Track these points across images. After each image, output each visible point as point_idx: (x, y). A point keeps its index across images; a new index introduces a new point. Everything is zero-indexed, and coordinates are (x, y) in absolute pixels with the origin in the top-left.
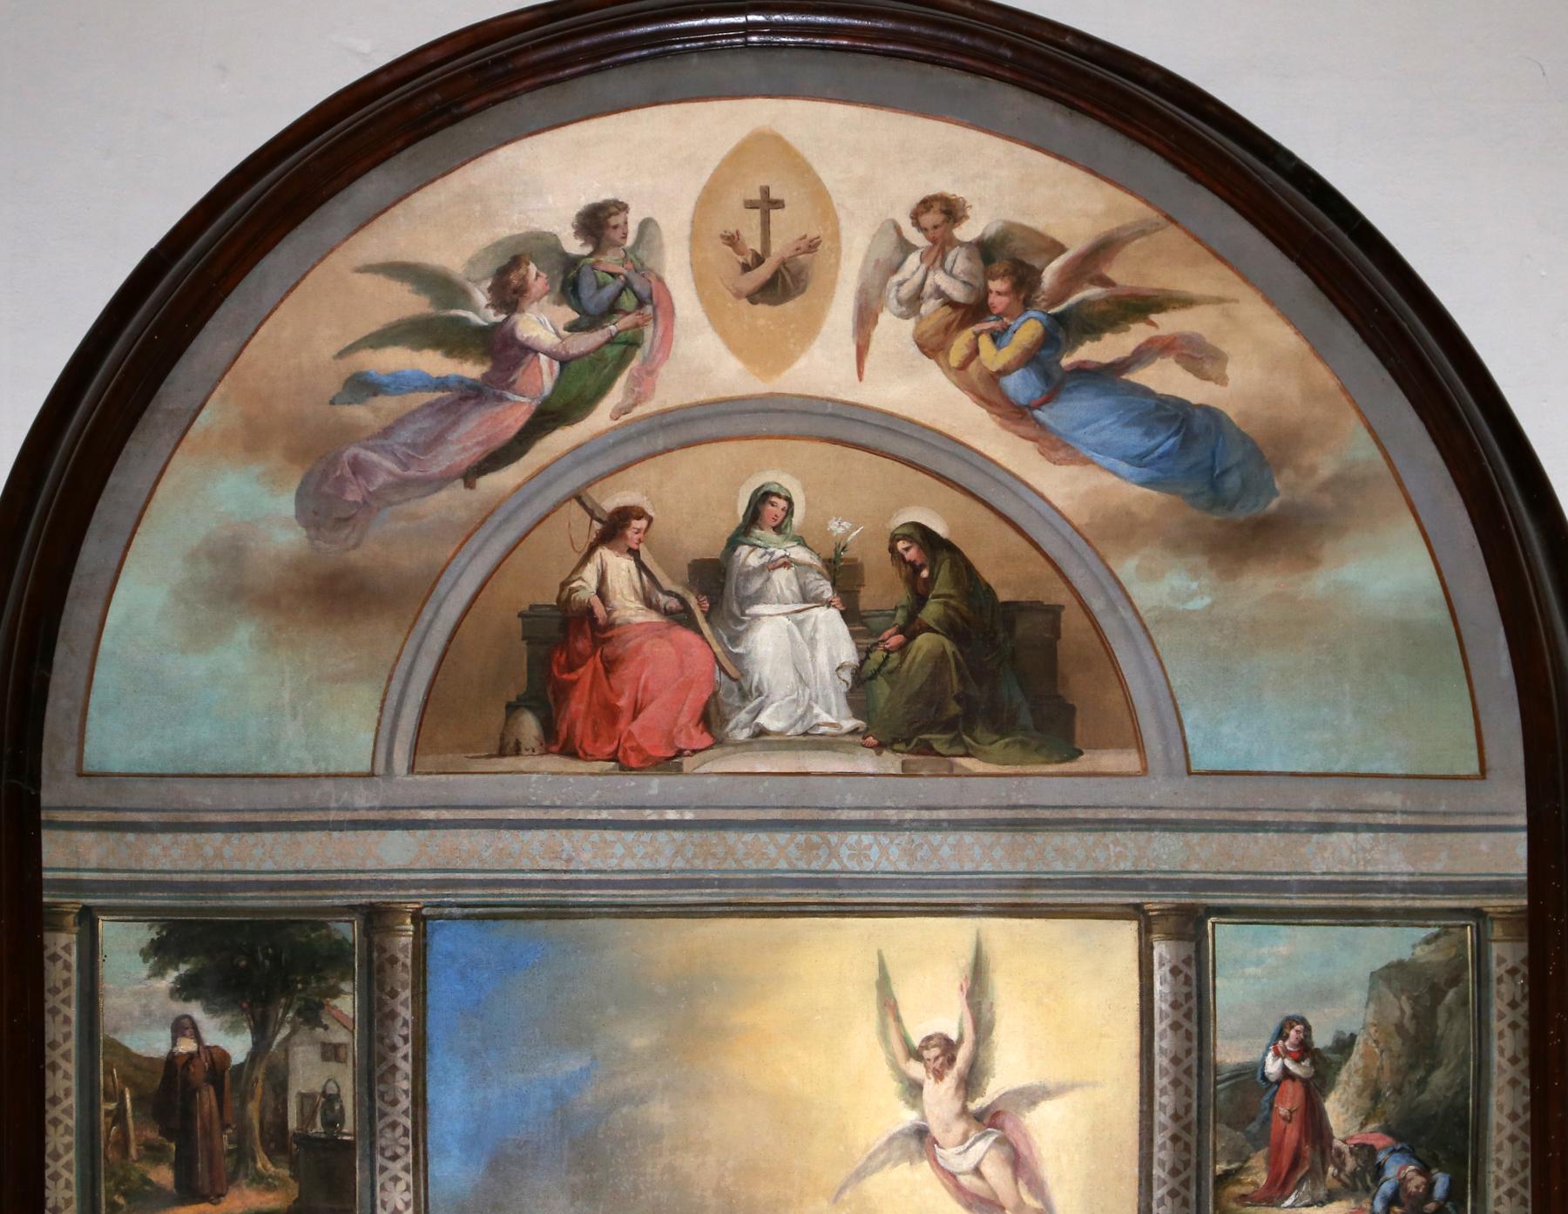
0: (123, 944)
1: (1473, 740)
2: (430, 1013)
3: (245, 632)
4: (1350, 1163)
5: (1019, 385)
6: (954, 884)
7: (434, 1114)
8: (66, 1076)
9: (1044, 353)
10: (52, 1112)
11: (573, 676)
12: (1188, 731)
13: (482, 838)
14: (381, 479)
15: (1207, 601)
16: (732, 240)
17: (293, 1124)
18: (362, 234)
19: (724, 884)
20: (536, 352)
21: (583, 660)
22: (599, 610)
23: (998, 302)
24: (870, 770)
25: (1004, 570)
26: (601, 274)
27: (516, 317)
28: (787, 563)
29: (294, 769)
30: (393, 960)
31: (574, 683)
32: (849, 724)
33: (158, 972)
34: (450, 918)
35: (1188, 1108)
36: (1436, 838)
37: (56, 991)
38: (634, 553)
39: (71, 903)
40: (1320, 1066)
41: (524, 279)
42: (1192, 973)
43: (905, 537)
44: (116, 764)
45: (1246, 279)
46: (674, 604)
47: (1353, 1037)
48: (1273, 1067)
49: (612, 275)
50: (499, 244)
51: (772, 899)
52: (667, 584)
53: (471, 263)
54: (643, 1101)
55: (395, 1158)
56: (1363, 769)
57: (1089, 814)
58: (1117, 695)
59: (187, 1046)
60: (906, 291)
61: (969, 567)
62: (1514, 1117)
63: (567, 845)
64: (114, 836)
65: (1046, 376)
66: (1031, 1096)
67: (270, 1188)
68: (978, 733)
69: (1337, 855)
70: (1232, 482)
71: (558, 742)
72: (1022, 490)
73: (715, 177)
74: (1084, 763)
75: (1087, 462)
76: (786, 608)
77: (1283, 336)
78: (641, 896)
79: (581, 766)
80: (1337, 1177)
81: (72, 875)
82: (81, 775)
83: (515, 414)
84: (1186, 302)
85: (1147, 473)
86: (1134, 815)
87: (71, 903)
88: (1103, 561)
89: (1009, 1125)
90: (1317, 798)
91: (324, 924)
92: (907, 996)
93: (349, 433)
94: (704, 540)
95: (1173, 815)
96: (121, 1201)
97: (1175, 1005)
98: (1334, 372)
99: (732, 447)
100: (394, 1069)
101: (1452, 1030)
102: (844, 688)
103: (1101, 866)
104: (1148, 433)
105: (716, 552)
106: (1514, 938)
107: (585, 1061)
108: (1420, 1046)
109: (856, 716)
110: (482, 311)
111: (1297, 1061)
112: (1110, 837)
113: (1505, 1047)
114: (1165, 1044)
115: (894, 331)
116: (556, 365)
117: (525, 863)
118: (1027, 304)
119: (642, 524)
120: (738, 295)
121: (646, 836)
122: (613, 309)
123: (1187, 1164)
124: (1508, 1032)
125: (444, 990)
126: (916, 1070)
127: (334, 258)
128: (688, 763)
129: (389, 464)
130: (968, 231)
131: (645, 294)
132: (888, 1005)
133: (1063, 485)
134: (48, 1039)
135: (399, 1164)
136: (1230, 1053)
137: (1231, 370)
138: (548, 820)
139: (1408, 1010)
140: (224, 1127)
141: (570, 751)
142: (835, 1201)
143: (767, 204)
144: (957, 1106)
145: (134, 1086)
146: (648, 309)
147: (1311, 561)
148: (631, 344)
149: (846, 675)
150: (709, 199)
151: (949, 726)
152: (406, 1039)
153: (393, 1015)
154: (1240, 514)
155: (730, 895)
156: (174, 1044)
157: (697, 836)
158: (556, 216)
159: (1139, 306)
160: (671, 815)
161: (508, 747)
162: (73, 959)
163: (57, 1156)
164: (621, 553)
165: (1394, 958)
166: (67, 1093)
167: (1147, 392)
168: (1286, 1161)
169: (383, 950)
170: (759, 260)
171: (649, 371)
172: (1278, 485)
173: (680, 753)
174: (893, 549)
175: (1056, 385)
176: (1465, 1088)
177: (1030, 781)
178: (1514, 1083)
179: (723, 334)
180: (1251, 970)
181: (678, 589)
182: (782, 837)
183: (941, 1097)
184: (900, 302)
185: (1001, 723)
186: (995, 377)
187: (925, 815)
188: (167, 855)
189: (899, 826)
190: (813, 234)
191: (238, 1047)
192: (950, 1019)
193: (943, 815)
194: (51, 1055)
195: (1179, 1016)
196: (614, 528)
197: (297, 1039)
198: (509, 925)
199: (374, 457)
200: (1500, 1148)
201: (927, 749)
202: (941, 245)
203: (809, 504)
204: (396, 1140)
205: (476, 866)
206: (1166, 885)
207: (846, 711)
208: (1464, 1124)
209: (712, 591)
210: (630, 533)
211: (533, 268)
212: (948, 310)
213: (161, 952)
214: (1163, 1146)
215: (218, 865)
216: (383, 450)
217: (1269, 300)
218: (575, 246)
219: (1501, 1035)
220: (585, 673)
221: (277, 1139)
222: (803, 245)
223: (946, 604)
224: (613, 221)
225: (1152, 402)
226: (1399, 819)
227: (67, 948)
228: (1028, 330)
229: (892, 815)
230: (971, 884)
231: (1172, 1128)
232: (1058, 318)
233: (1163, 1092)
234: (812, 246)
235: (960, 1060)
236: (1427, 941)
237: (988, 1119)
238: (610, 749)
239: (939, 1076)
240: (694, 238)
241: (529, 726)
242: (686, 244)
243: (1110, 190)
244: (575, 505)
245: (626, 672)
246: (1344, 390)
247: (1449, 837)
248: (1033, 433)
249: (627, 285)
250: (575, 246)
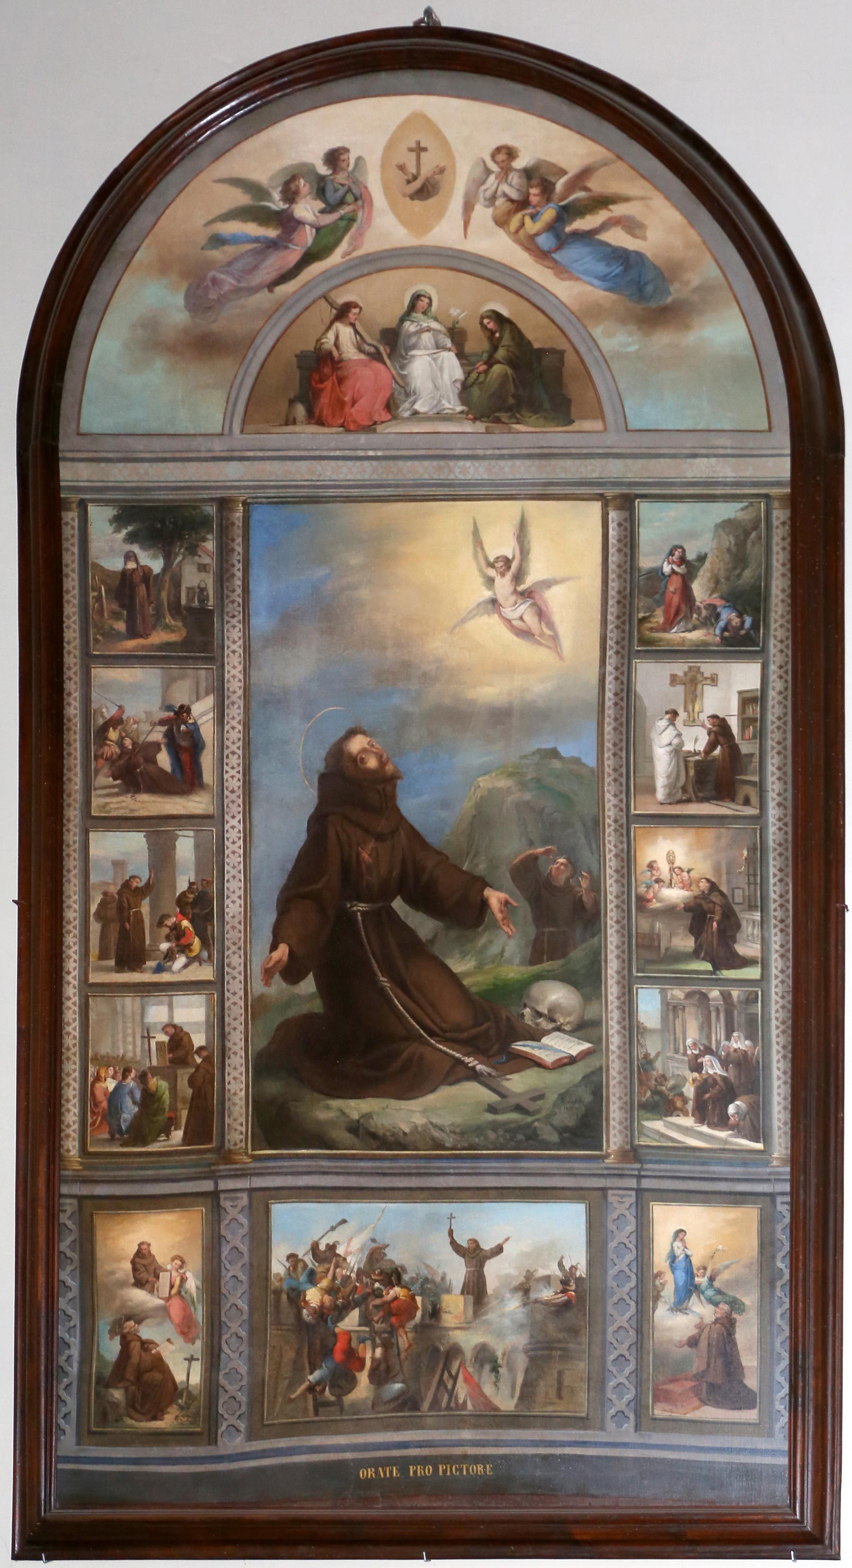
0: (100, 518)
1: (765, 414)
2: (251, 549)
3: (160, 363)
4: (704, 613)
5: (545, 241)
6: (511, 485)
7: (253, 596)
8: (73, 580)
9: (557, 225)
10: (66, 597)
11: (322, 386)
12: (626, 410)
13: (276, 464)
14: (226, 288)
15: (637, 347)
16: (402, 168)
17: (183, 601)
18: (213, 166)
19: (397, 486)
20: (304, 224)
21: (328, 378)
22: (335, 353)
23: (534, 199)
24: (470, 430)
25: (536, 332)
26: (336, 184)
27: (294, 206)
28: (429, 330)
29: (182, 431)
30: (233, 524)
31: (322, 390)
32: (459, 408)
33: (117, 530)
34: (261, 503)
35: (625, 588)
36: (748, 460)
37: (67, 540)
38: (353, 325)
39: (75, 497)
40: (690, 569)
41: (298, 187)
42: (628, 525)
43: (488, 317)
44: (96, 428)
45: (656, 187)
46: (372, 350)
47: (706, 555)
48: (667, 569)
49: (342, 185)
50: (285, 169)
51: (420, 493)
52: (369, 340)
53: (272, 178)
54: (356, 589)
55: (233, 617)
56: (712, 428)
57: (578, 451)
58: (591, 394)
59: (131, 565)
60: (489, 194)
61: (519, 332)
62: (783, 591)
63: (319, 468)
64: (95, 464)
65: (558, 236)
66: (548, 584)
67: (173, 631)
68: (524, 412)
69: (699, 469)
70: (649, 288)
71: (315, 418)
72: (545, 293)
73: (395, 133)
74: (575, 426)
75: (578, 279)
76: (428, 352)
77: (674, 216)
78: (356, 492)
79: (326, 430)
80: (698, 619)
81: (75, 484)
82: (79, 434)
83: (293, 256)
84: (626, 199)
85: (607, 284)
86: (600, 451)
87: (75, 497)
88: (585, 327)
89: (537, 597)
90: (690, 442)
91: (198, 507)
92: (487, 538)
93: (210, 265)
94: (387, 317)
95: (619, 451)
96: (100, 638)
97: (619, 541)
98: (700, 234)
99: (402, 272)
100: (233, 575)
101: (754, 551)
102: (457, 391)
103: (584, 475)
104: (608, 265)
105: (394, 325)
106: (783, 508)
107: (327, 571)
108: (738, 558)
109: (463, 404)
110: (277, 203)
111: (679, 566)
112: (588, 461)
113: (780, 559)
114: (614, 559)
115: (482, 214)
116: (314, 231)
117: (298, 477)
118: (548, 200)
119: (356, 311)
120: (405, 196)
121: (358, 463)
122: (342, 202)
123: (624, 614)
124: (781, 552)
125: (257, 537)
126: (492, 572)
127: (203, 176)
128: (379, 428)
129: (233, 281)
130: (519, 163)
131: (358, 194)
132: (478, 542)
133: (566, 291)
134: (64, 562)
135: (236, 619)
136: (646, 562)
137: (650, 234)
138: (310, 456)
139: (733, 542)
140: (150, 603)
141: (321, 423)
142: (451, 632)
143: (419, 149)
144: (512, 588)
145: (106, 584)
146: (360, 203)
147: (687, 327)
148: (351, 220)
149: (459, 385)
150: (390, 146)
151: (509, 409)
152: (239, 561)
153: (233, 550)
154: (653, 305)
155: (400, 491)
156: (125, 564)
157: (384, 463)
158: (313, 155)
159: (603, 202)
160: (371, 453)
161: (290, 421)
162: (76, 524)
163: (69, 618)
164: (346, 325)
165: (726, 517)
166: (74, 588)
167: (607, 244)
168: (673, 611)
169: (228, 519)
170: (415, 178)
171: (360, 234)
172: (671, 289)
173: (375, 423)
174: (481, 323)
175: (563, 241)
176: (760, 577)
177: (548, 435)
178: (783, 575)
179: (397, 215)
180: (656, 524)
181: (375, 343)
182: (426, 463)
183: (503, 585)
184: (485, 199)
185: (535, 407)
186: (532, 238)
187: (497, 452)
188: (121, 474)
189: (484, 458)
190: (442, 164)
191: (156, 565)
192: (509, 549)
193: (506, 452)
194: (65, 570)
195: (621, 546)
196: (343, 312)
197: (186, 561)
198: (290, 506)
199: (222, 276)
200: (776, 605)
201: (498, 421)
202: (506, 170)
203: (440, 300)
204: (234, 608)
205: (274, 478)
206: (615, 484)
207: (458, 402)
208: (759, 594)
209: (392, 343)
210: (351, 315)
211: (302, 182)
212: (509, 203)
213: (119, 521)
214: (613, 606)
215: (146, 479)
216: (228, 273)
217: (667, 198)
218: (323, 170)
219: (778, 553)
220: (328, 384)
221: (176, 608)
222: (437, 171)
223: (508, 350)
224: (342, 157)
225: (609, 250)
226: (729, 451)
227: (73, 519)
228: (549, 214)
229: (480, 452)
230: (519, 485)
231: (617, 597)
232: (565, 208)
233: (613, 581)
234: (442, 171)
235: (513, 568)
236: (743, 509)
237: (527, 595)
238: (341, 421)
239: (503, 575)
240: (384, 166)
241: (300, 410)
242: (378, 169)
243: (589, 143)
244: (323, 301)
245: (348, 384)
246: (704, 242)
247: (753, 460)
248: (551, 265)
249: (349, 190)
250: (323, 170)
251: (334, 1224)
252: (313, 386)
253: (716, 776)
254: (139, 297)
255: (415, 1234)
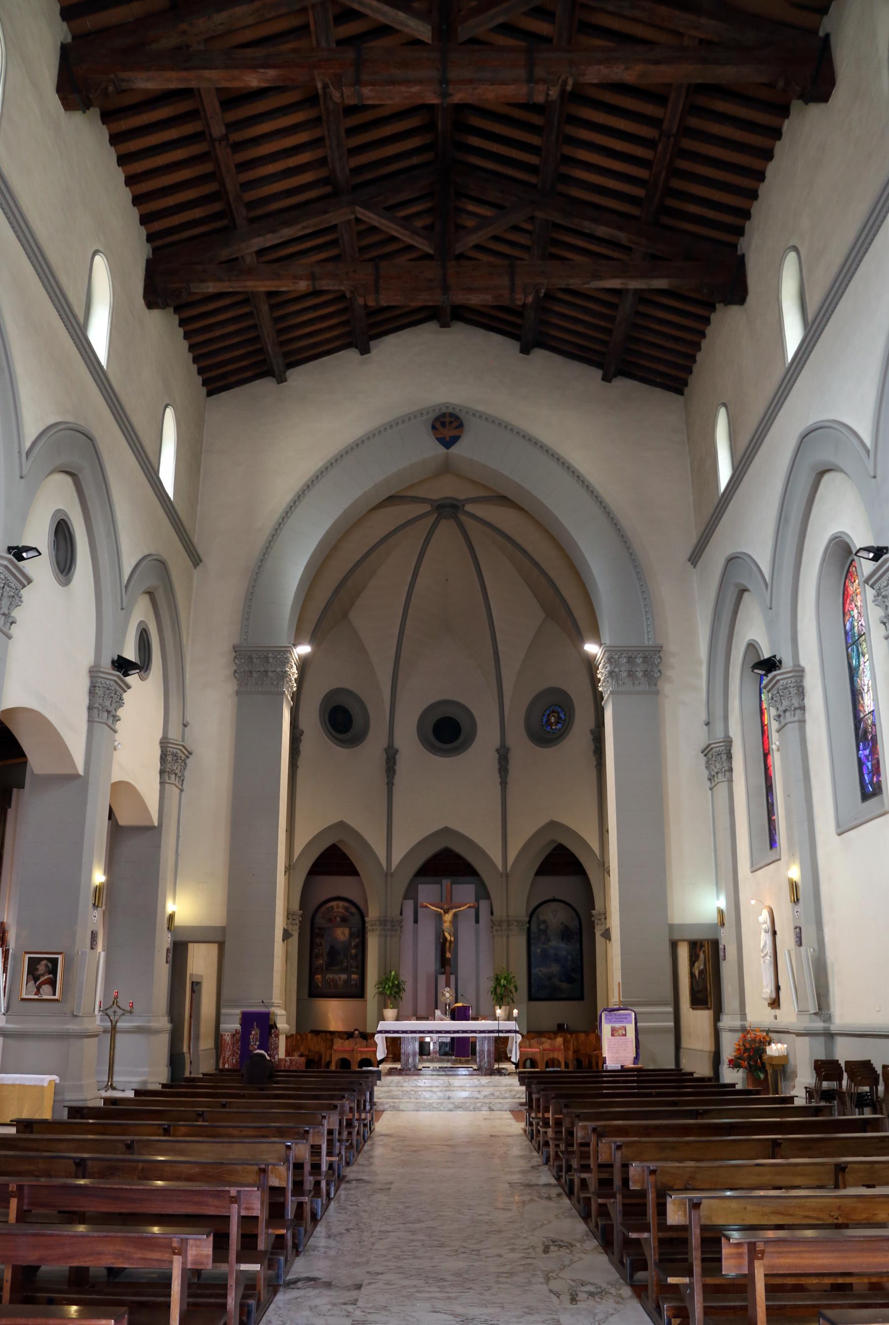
26: (332, 907)
209: (335, 917)
251: (704, 717)
252: (330, 920)
253: (356, 946)
254: (319, 915)
255: (336, 977)
